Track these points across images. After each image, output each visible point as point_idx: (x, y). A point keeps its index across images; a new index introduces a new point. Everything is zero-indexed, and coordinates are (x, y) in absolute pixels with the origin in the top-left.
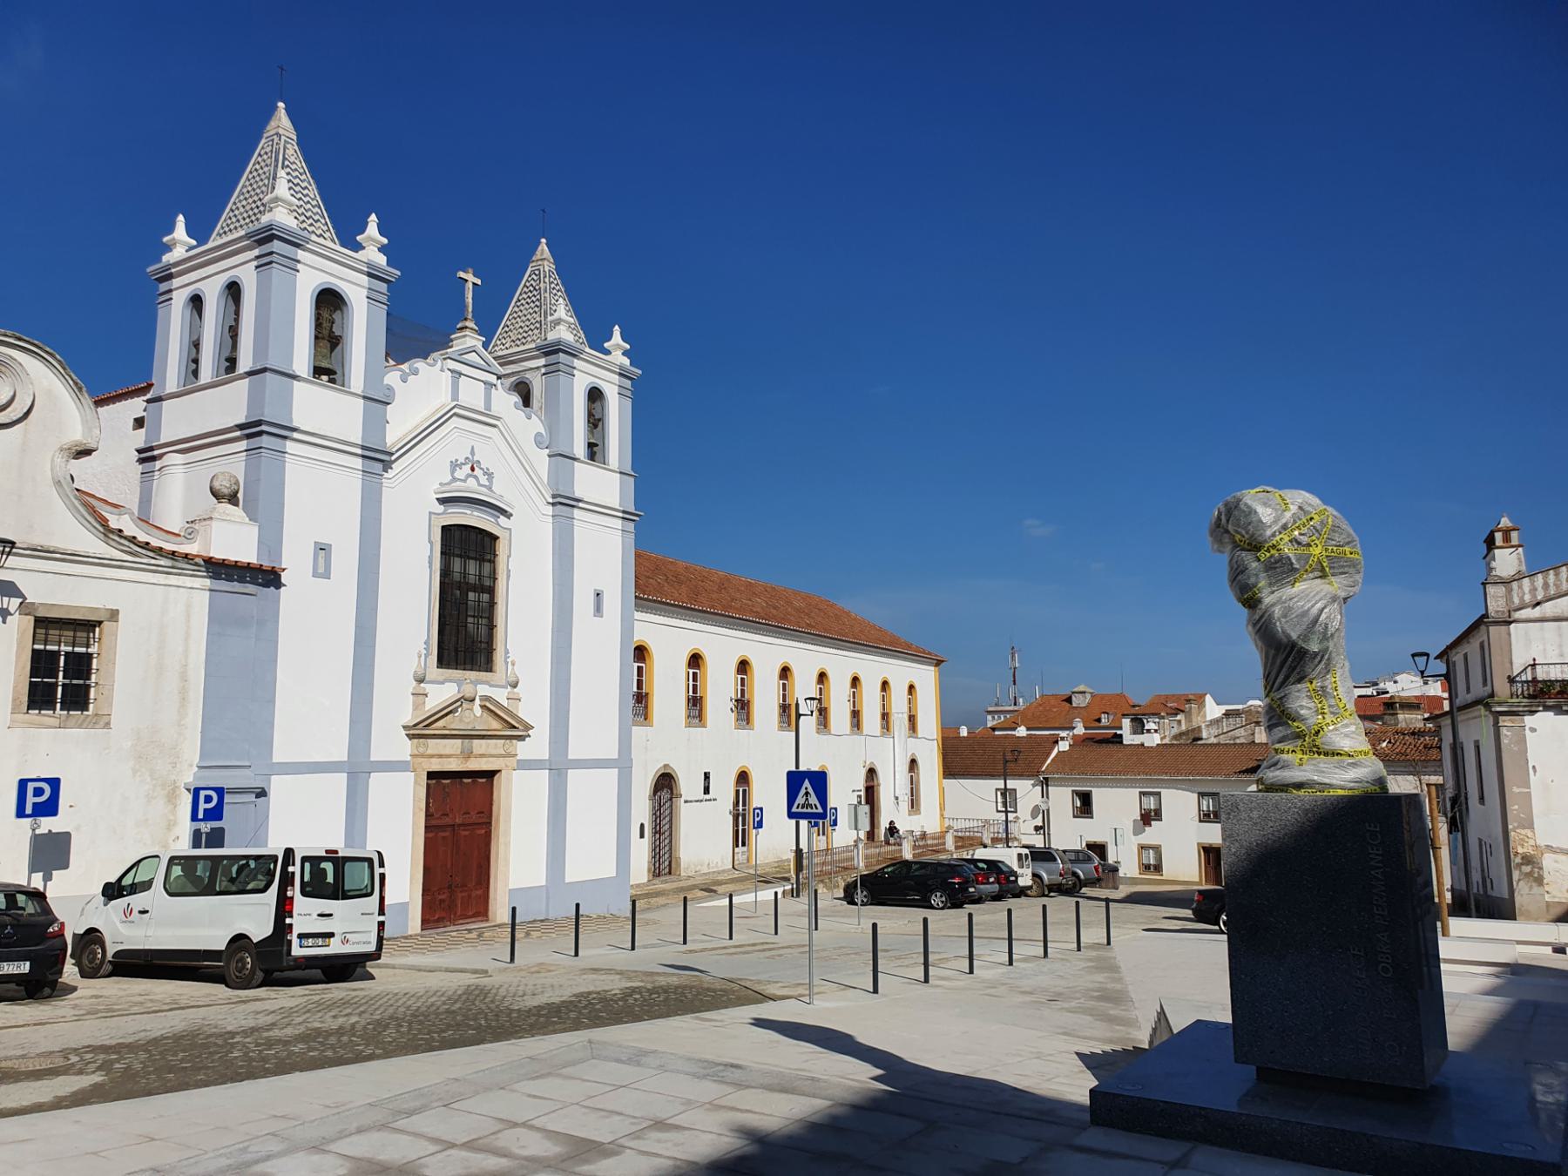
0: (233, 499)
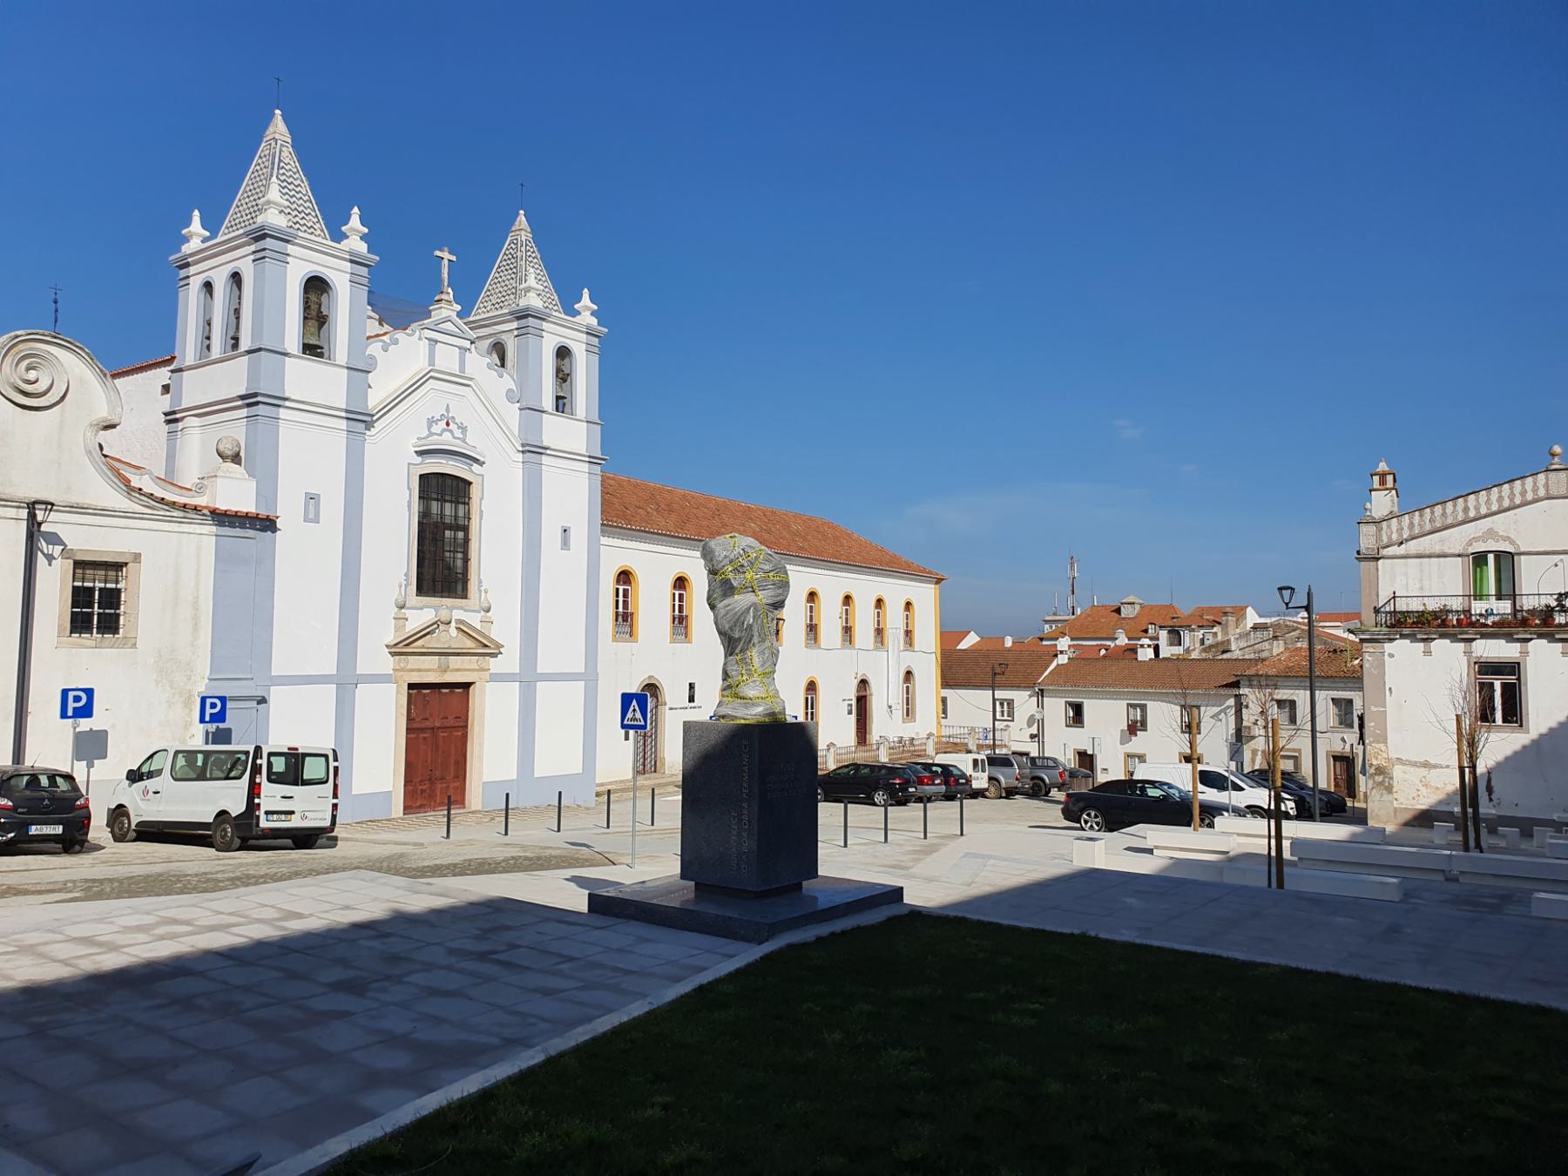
0: (236, 458)
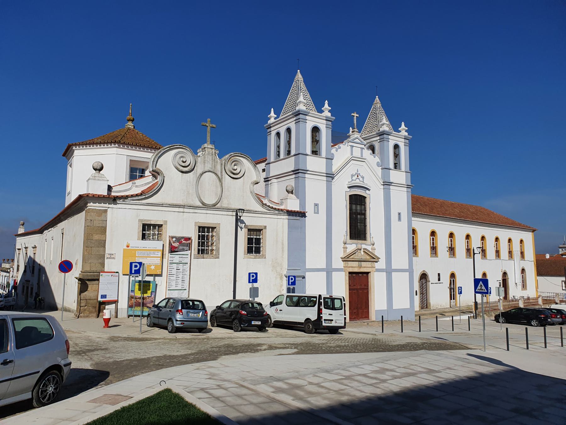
0: (292, 193)
